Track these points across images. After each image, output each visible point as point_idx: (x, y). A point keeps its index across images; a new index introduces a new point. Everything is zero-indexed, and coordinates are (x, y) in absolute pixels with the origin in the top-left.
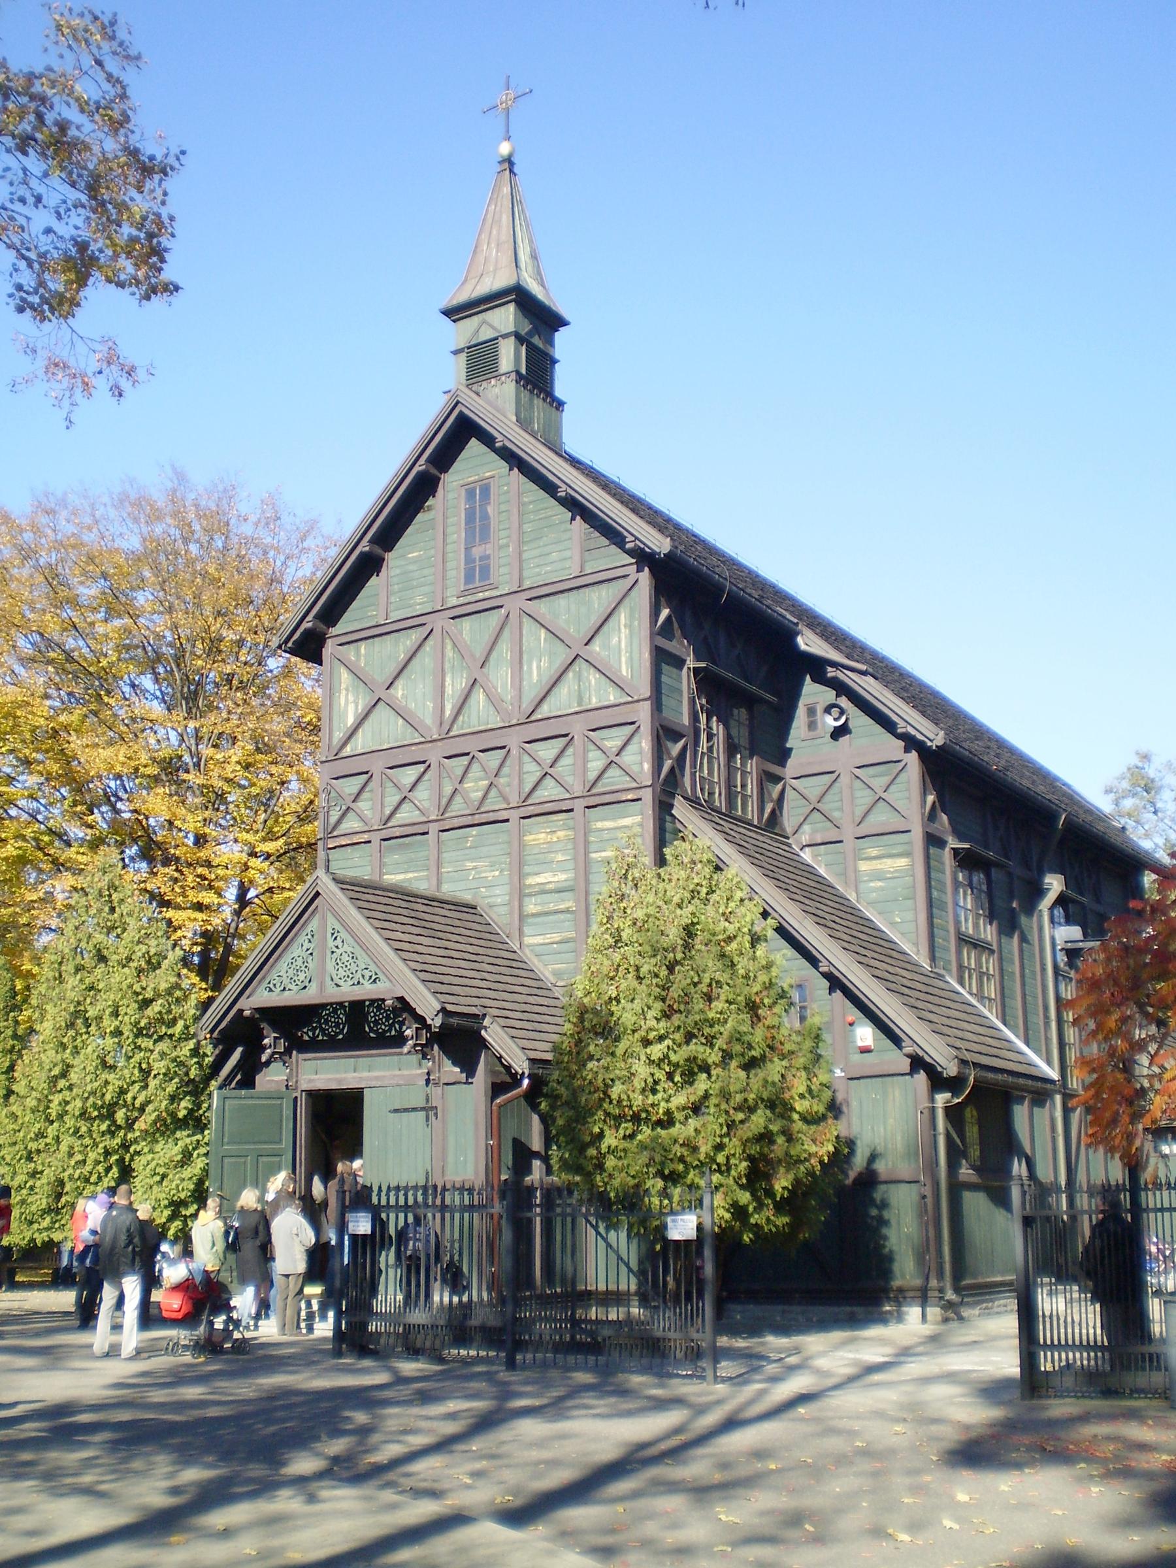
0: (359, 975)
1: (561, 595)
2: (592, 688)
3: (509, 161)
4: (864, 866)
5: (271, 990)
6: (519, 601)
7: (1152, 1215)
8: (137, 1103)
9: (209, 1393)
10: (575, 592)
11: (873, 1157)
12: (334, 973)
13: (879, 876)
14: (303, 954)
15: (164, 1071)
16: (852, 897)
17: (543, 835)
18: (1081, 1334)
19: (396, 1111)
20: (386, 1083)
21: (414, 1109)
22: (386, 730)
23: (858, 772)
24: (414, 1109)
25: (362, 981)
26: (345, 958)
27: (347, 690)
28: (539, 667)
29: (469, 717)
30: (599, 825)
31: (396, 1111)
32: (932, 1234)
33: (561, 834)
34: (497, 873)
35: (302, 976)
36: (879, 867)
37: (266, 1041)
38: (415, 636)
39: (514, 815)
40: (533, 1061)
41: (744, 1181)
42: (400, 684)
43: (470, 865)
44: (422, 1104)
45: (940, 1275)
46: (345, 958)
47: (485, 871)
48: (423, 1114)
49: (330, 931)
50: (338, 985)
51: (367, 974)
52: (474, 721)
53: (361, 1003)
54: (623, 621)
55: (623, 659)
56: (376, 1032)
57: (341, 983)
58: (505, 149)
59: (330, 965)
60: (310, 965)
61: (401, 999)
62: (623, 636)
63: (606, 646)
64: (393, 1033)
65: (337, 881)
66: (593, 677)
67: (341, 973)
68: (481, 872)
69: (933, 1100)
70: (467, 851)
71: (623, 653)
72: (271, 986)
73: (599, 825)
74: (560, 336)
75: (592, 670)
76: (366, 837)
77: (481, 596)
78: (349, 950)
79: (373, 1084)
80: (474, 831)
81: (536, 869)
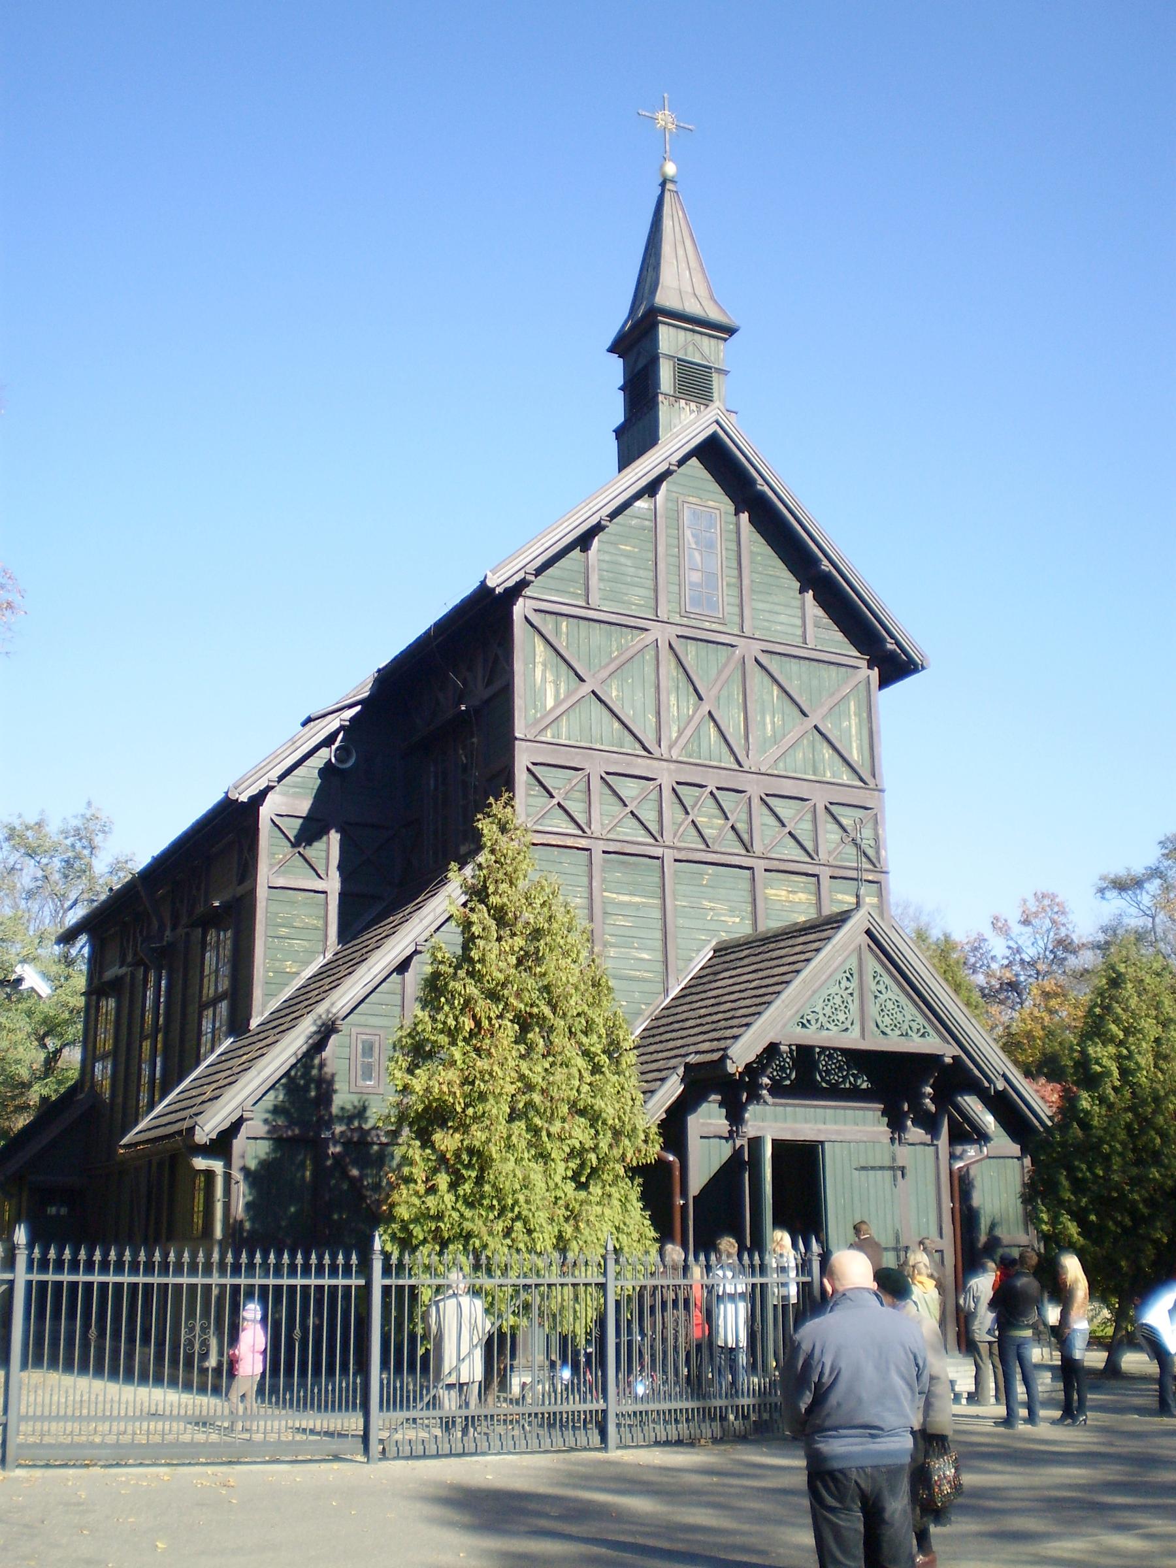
1: (793, 660)
5: (804, 1025)
7: (730, 1307)
9: (1104, 1444)
10: (807, 662)
14: (841, 992)
17: (784, 893)
19: (864, 1168)
20: (848, 1138)
21: (881, 1168)
24: (881, 1168)
25: (910, 1032)
28: (773, 723)
31: (864, 1168)
34: (737, 920)
43: (706, 903)
44: (887, 1163)
46: (890, 1005)
48: (888, 1174)
51: (915, 1026)
53: (810, 1049)
55: (854, 745)
56: (827, 1082)
57: (888, 1031)
59: (873, 1010)
60: (850, 1006)
61: (32, 988)
62: (853, 722)
64: (848, 1085)
67: (887, 1020)
70: (703, 889)
71: (854, 739)
72: (805, 1021)
75: (825, 744)
76: (583, 843)
77: (707, 625)
78: (894, 997)
79: (833, 1138)
80: (711, 869)
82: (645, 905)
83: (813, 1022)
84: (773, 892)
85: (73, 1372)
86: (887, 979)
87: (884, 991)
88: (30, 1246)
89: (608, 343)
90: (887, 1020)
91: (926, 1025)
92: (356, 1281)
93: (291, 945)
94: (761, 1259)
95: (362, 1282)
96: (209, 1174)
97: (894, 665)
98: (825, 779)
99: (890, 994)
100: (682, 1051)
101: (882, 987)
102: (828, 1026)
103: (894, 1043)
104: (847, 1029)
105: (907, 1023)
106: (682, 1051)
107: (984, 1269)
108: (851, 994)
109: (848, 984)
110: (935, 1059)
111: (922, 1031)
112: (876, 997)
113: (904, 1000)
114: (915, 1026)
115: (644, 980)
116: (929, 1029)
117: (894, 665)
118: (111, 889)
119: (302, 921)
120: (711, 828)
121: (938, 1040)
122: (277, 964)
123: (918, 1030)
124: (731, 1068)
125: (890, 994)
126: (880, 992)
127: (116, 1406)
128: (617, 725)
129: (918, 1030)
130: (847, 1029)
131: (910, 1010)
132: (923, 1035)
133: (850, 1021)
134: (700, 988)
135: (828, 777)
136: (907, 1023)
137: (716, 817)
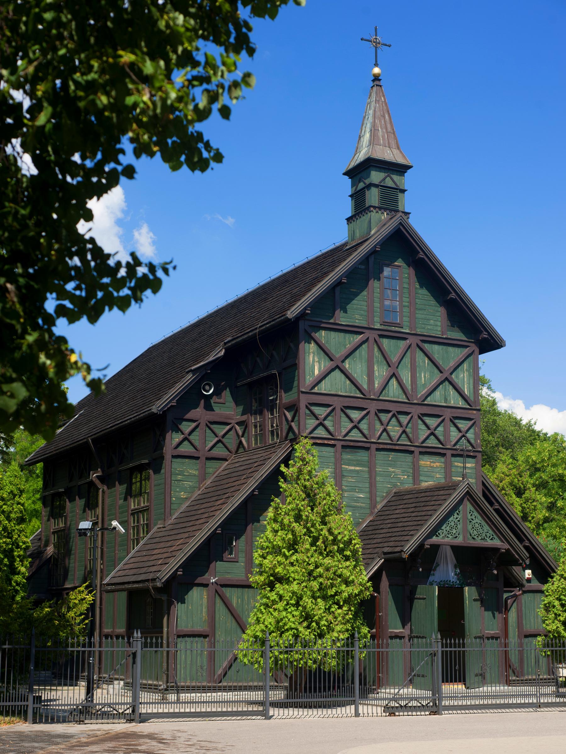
2: (451, 396)
3: (376, 78)
6: (416, 340)
12: (472, 532)
14: (454, 520)
22: (336, 384)
27: (314, 353)
28: (425, 377)
29: (388, 391)
30: (456, 464)
33: (438, 464)
34: (406, 477)
35: (454, 531)
38: (358, 338)
39: (417, 450)
42: (347, 361)
45: (89, 663)
46: (477, 525)
49: (468, 511)
50: (473, 538)
52: (391, 394)
54: (465, 368)
55: (466, 386)
57: (475, 537)
58: (376, 70)
60: (459, 526)
62: (465, 374)
63: (457, 377)
66: (452, 392)
71: (466, 383)
73: (456, 464)
75: (451, 387)
76: (332, 442)
78: (479, 522)
81: (426, 479)
82: (361, 471)
83: (441, 534)
84: (423, 462)
86: (476, 514)
87: (474, 519)
88: (442, 639)
89: (344, 171)
90: (475, 532)
91: (494, 534)
93: (183, 484)
94: (463, 641)
97: (490, 342)
98: (450, 405)
99: (477, 520)
100: (381, 545)
101: (473, 517)
102: (448, 535)
103: (479, 542)
104: (456, 537)
106: (381, 545)
108: (459, 521)
109: (457, 516)
110: (495, 550)
111: (491, 537)
112: (470, 522)
113: (483, 523)
114: (488, 535)
115: (361, 507)
116: (495, 536)
117: (490, 342)
119: (188, 472)
120: (394, 432)
121: (499, 541)
122: (177, 494)
124: (190, 129)
125: (477, 520)
126: (472, 519)
128: (348, 382)
130: (456, 537)
131: (486, 527)
132: (492, 539)
133: (457, 533)
134: (388, 512)
135: (452, 403)
137: (396, 426)
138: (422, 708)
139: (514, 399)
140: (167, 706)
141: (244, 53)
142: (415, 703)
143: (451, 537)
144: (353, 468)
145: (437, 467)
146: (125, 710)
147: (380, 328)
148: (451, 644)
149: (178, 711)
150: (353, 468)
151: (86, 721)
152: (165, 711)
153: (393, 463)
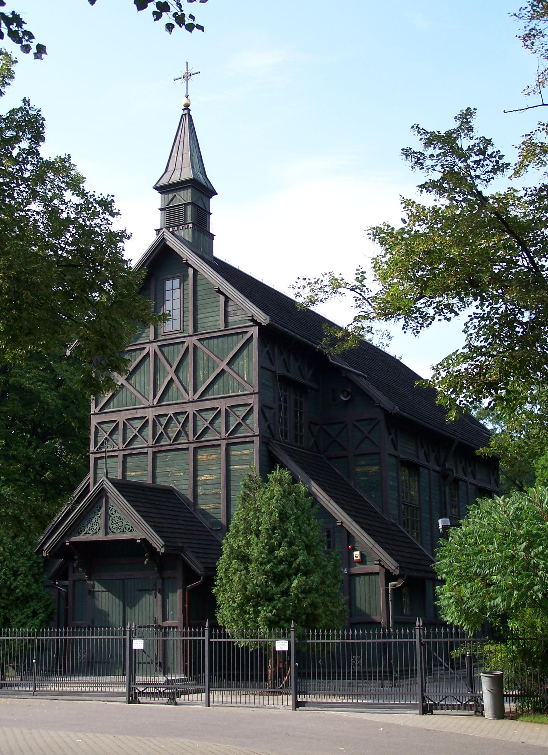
0: (123, 527)
4: (358, 470)
8: (12, 587)
11: (9, 84)
13: (365, 474)
15: (24, 572)
16: (352, 484)
18: (210, 549)
23: (355, 423)
26: (116, 519)
32: (288, 367)
34: (182, 474)
35: (95, 527)
36: (365, 470)
37: (76, 557)
40: (206, 568)
41: (304, 624)
46: (116, 519)
47: (176, 473)
50: (113, 532)
51: (127, 527)
55: (245, 373)
60: (99, 522)
65: (111, 480)
67: (115, 526)
68: (174, 473)
69: (387, 585)
74: (213, 201)
78: (118, 515)
81: (203, 472)
85: (32, 674)
87: (114, 513)
90: (115, 526)
92: (211, 640)
95: (211, 640)
96: (424, 638)
99: (117, 514)
104: (97, 532)
105: (124, 526)
107: (92, 593)
114: (127, 527)
118: (401, 358)
123: (129, 529)
126: (112, 514)
127: (396, 698)
129: (129, 529)
130: (97, 532)
132: (131, 531)
136: (124, 526)
138: (160, 694)
139: (398, 360)
140: (508, 699)
141: (184, 108)
142: (153, 690)
143: (92, 533)
144: (134, 474)
145: (213, 459)
146: (441, 701)
147: (162, 338)
148: (195, 632)
149: (311, 701)
150: (134, 474)
151: (435, 712)
152: (323, 701)
153: (171, 462)
